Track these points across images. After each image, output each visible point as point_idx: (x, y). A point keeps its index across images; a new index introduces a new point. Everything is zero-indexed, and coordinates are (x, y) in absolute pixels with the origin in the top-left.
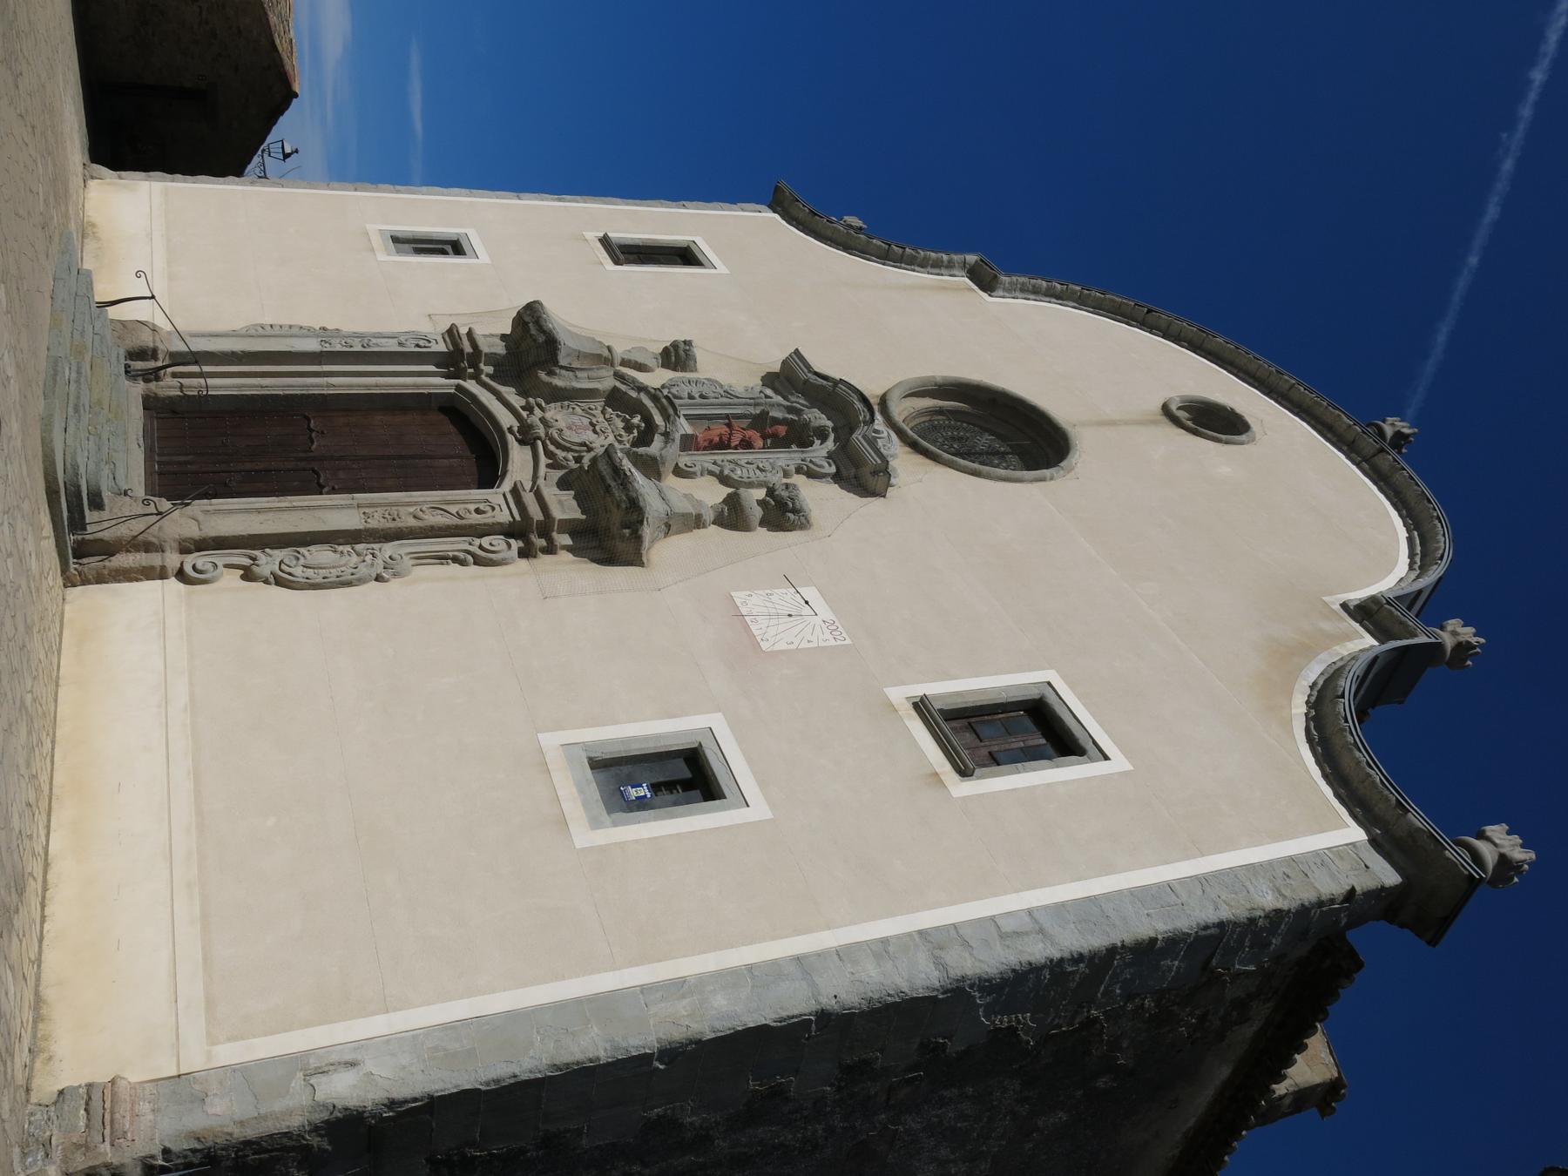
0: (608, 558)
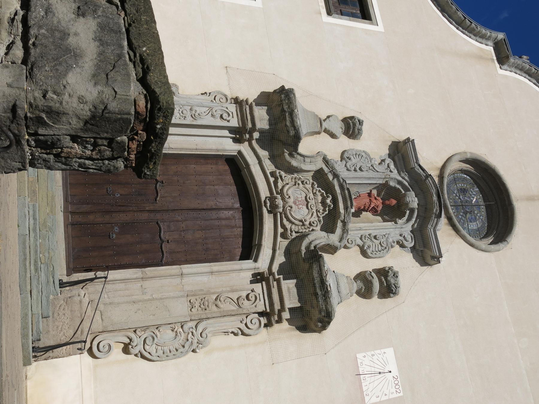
0: (304, 328)
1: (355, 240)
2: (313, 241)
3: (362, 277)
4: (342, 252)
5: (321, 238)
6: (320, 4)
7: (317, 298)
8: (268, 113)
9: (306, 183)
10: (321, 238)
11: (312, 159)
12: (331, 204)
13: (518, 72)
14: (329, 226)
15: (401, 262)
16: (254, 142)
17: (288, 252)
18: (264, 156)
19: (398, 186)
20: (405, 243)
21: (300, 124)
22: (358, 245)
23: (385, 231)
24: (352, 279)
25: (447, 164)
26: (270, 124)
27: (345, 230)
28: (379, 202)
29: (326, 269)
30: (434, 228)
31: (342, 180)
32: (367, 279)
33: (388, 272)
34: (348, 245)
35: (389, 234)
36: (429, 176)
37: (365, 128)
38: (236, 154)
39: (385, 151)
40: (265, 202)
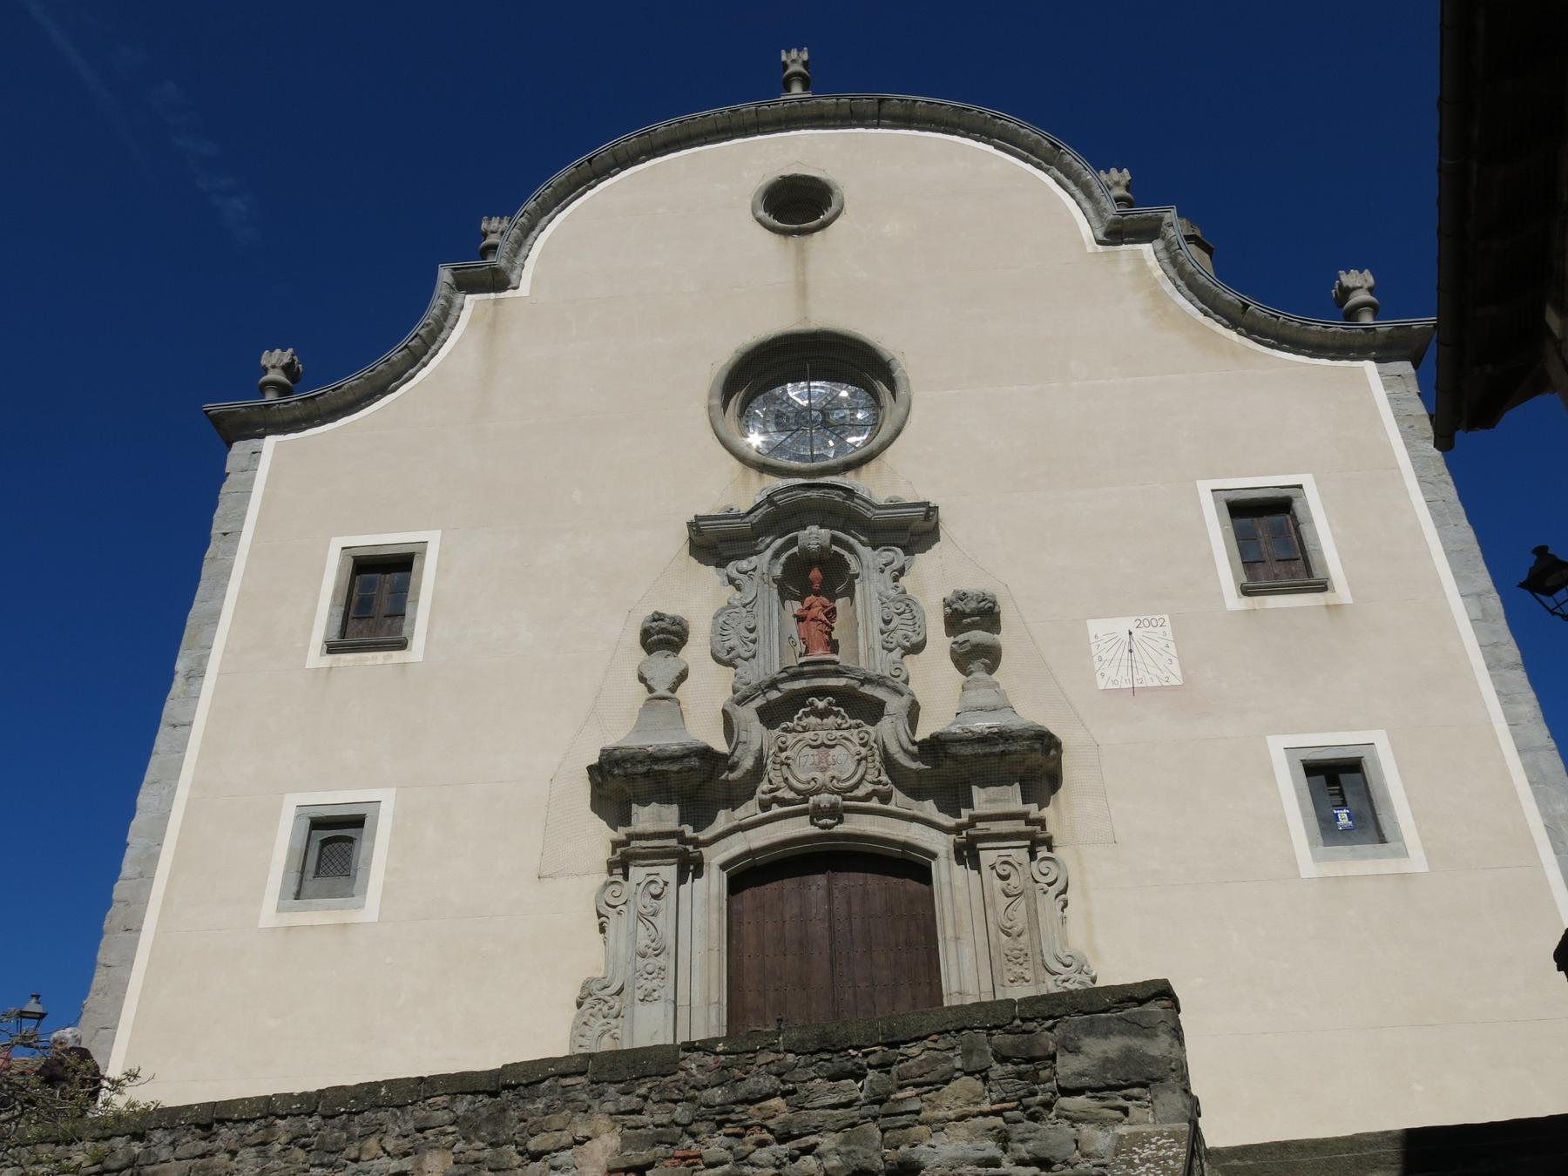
0: (1053, 780)
3: (964, 659)
5: (895, 728)
6: (380, 661)
7: (1010, 753)
8: (645, 803)
10: (895, 728)
13: (524, 251)
14: (872, 711)
15: (934, 578)
16: (704, 835)
17: (917, 794)
18: (728, 821)
20: (896, 565)
26: (670, 802)
27: (879, 682)
34: (903, 677)
36: (770, 499)
37: (670, 610)
39: (710, 575)
40: (822, 827)
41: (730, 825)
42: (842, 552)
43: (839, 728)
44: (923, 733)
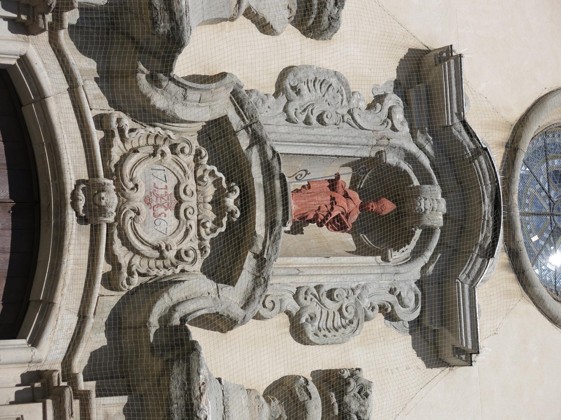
1: (281, 301)
2: (179, 303)
4: (249, 330)
5: (201, 296)
9: (182, 151)
10: (201, 296)
11: (204, 94)
12: (235, 208)
14: (222, 269)
15: (382, 356)
16: (63, 36)
17: (115, 324)
19: (405, 166)
20: (399, 310)
21: (187, 6)
22: (288, 313)
23: (355, 278)
24: (261, 393)
25: (532, 116)
27: (260, 279)
28: (352, 205)
29: (202, 381)
30: (473, 282)
31: (270, 153)
32: (295, 399)
33: (348, 384)
34: (264, 312)
35: (364, 287)
38: (13, 62)
39: (386, 74)
40: (74, 195)
41: (77, 72)
42: (413, 243)
43: (200, 224)
44: (197, 334)
